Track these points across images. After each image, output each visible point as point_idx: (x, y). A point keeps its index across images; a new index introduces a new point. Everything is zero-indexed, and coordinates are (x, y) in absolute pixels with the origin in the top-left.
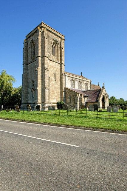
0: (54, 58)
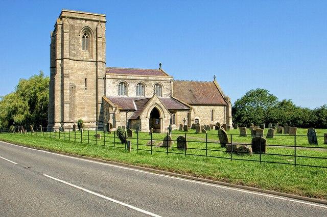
0: (86, 54)
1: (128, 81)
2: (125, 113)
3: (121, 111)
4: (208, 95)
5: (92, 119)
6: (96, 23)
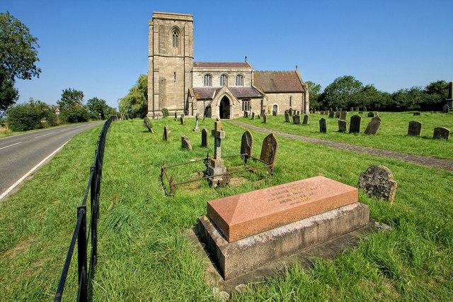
0: (175, 51)
1: (212, 73)
2: (203, 102)
3: (198, 100)
4: (284, 83)
5: (180, 108)
6: (183, 23)
